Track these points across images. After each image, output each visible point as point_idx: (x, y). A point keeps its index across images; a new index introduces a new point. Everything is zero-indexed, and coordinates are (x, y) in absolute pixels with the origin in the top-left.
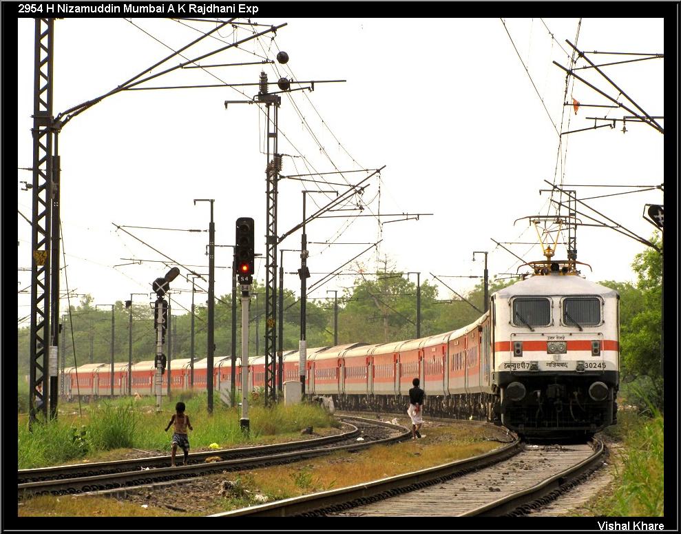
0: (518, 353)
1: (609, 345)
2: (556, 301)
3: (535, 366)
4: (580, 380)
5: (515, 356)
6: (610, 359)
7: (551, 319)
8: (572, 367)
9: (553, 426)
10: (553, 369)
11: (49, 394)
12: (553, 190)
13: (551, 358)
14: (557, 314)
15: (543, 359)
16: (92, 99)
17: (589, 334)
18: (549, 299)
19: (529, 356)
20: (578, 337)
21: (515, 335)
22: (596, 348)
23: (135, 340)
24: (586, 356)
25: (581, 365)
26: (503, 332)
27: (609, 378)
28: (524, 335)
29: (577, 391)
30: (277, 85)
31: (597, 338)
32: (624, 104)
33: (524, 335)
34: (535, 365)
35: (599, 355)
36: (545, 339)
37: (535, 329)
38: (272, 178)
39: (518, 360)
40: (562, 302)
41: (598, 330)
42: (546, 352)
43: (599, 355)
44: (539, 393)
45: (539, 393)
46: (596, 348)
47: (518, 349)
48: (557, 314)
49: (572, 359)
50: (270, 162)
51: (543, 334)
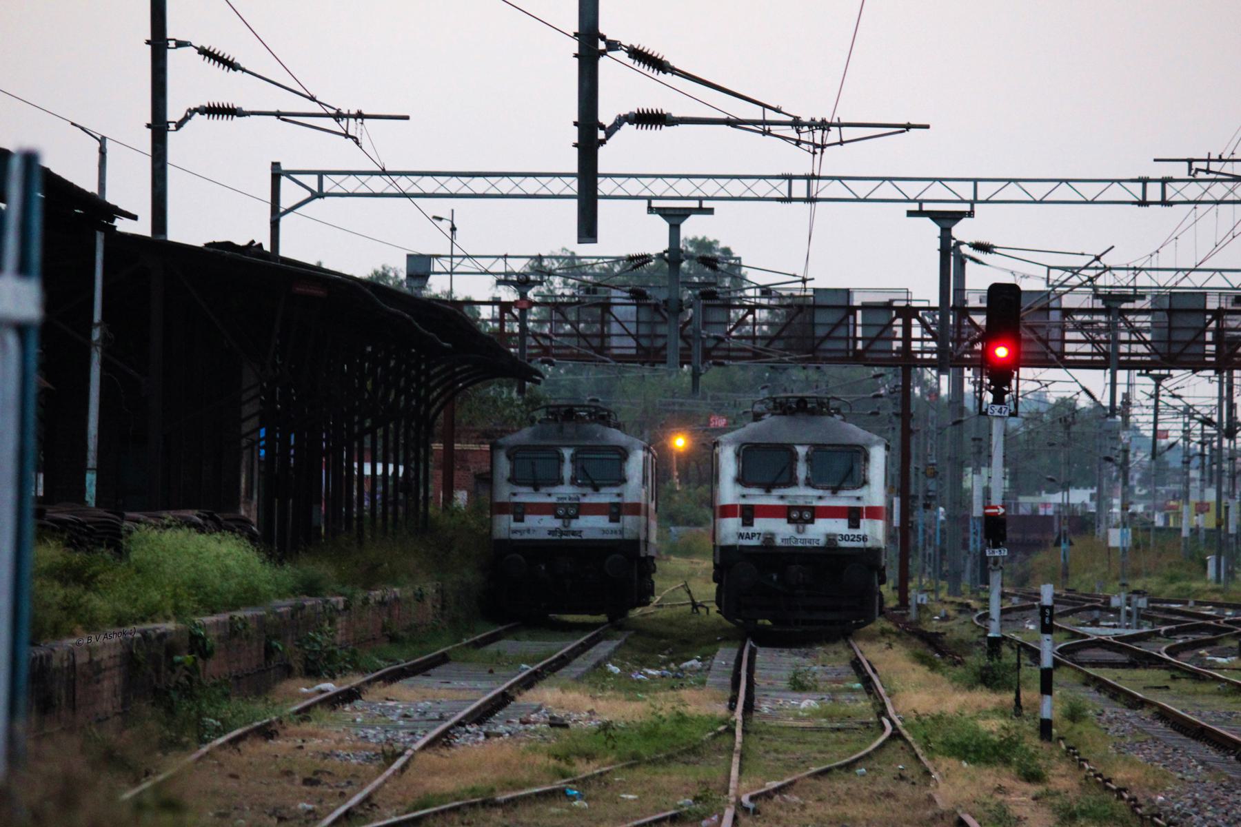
0: (748, 522)
1: (873, 513)
2: (802, 451)
3: (769, 537)
4: (830, 557)
6: (874, 532)
12: (972, 203)
15: (781, 530)
16: (331, 268)
19: (762, 525)
20: (772, 500)
22: (854, 516)
23: (20, 727)
24: (839, 526)
25: (831, 539)
26: (729, 492)
27: (868, 559)
28: (759, 498)
30: (447, 288)
31: (617, 500)
32: (912, 122)
33: (759, 498)
36: (553, 500)
38: (412, 455)
41: (858, 493)
44: (775, 577)
45: (775, 577)
46: (854, 516)
47: (748, 514)
49: (820, 530)
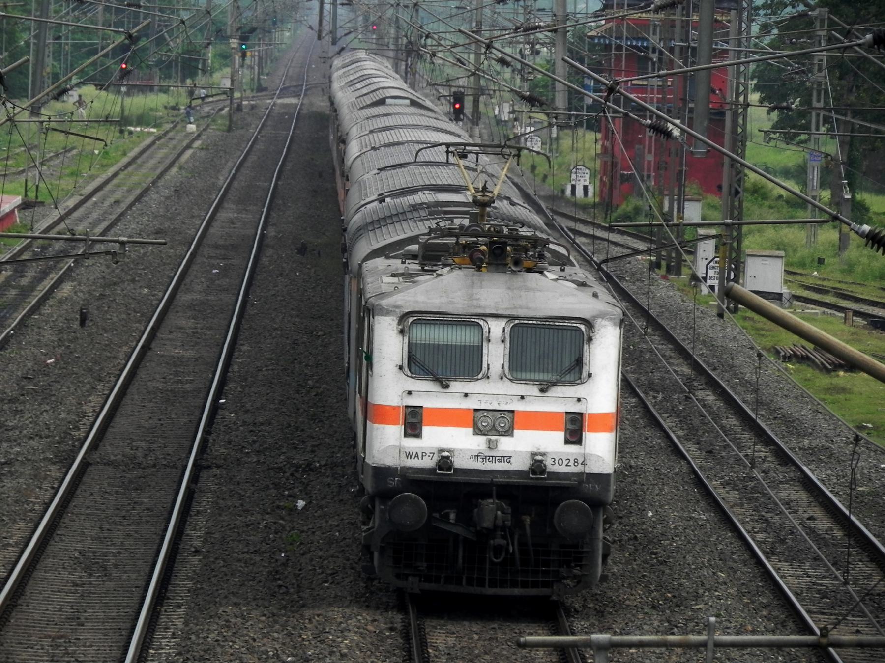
3: (538, 466)
4: (537, 494)
5: (406, 435)
6: (600, 450)
7: (485, 366)
8: (520, 464)
9: (532, 587)
10: (479, 465)
11: (853, 518)
13: (478, 443)
14: (496, 356)
15: (463, 445)
17: (560, 401)
18: (481, 322)
21: (410, 393)
28: (428, 396)
29: (530, 515)
34: (448, 457)
35: (418, 435)
37: (452, 384)
39: (412, 444)
40: (508, 330)
42: (471, 430)
43: (418, 435)
48: (496, 356)
49: (519, 448)
50: (747, 171)
51: (466, 395)
